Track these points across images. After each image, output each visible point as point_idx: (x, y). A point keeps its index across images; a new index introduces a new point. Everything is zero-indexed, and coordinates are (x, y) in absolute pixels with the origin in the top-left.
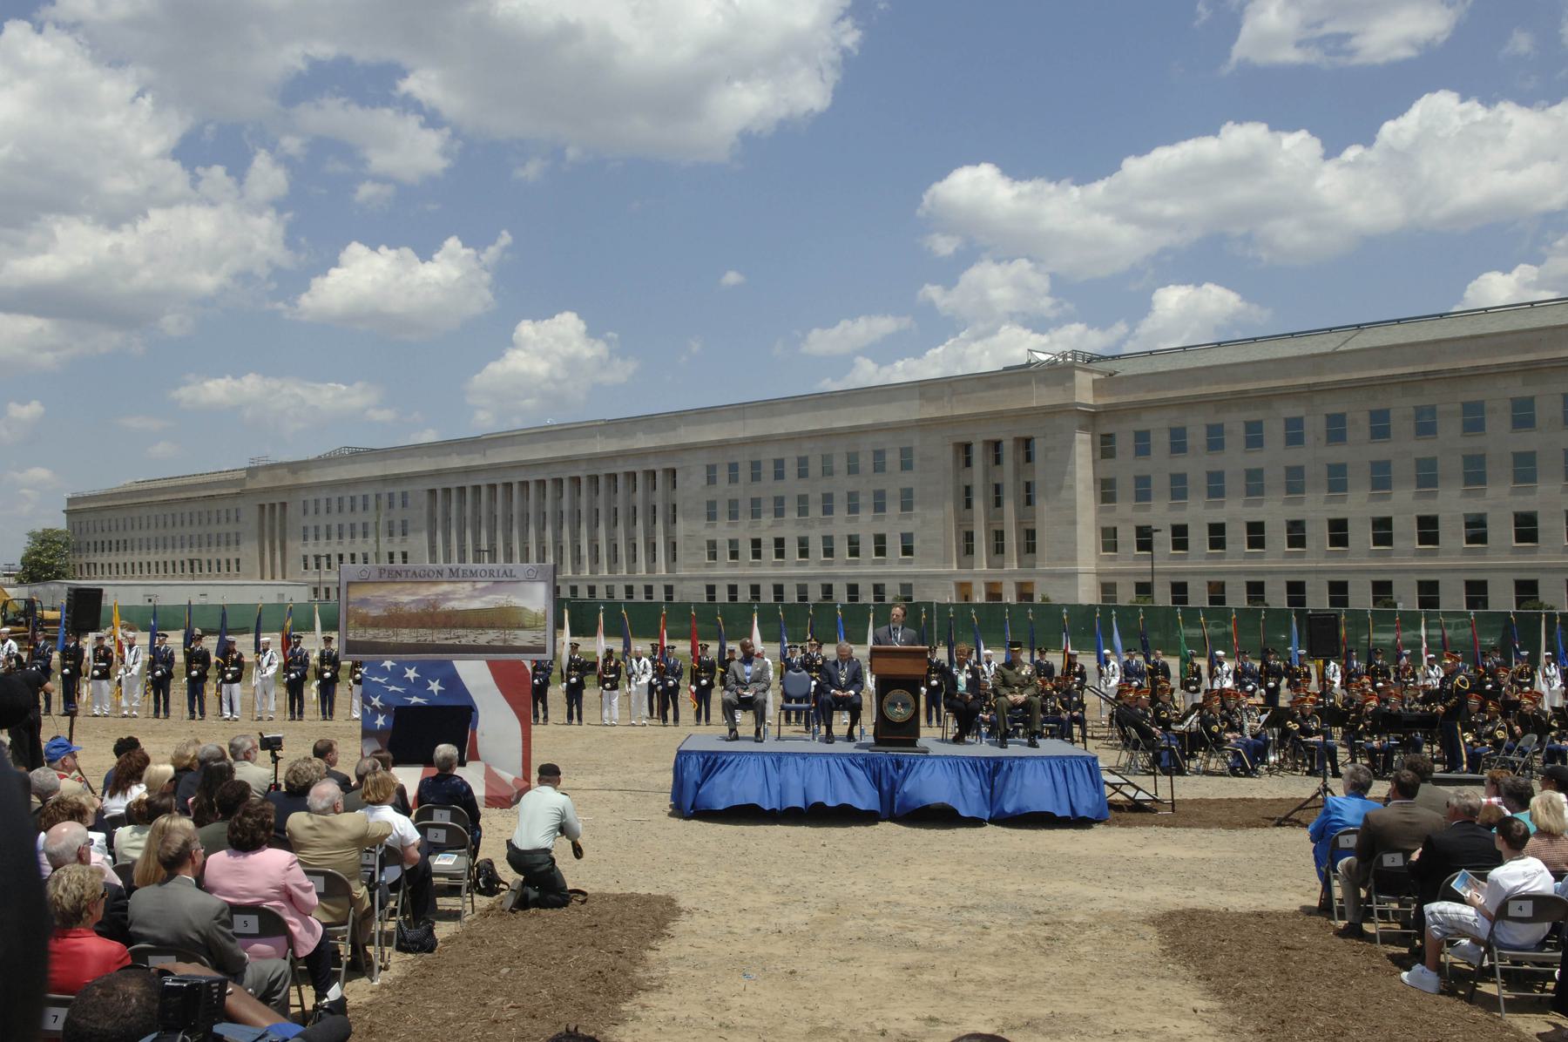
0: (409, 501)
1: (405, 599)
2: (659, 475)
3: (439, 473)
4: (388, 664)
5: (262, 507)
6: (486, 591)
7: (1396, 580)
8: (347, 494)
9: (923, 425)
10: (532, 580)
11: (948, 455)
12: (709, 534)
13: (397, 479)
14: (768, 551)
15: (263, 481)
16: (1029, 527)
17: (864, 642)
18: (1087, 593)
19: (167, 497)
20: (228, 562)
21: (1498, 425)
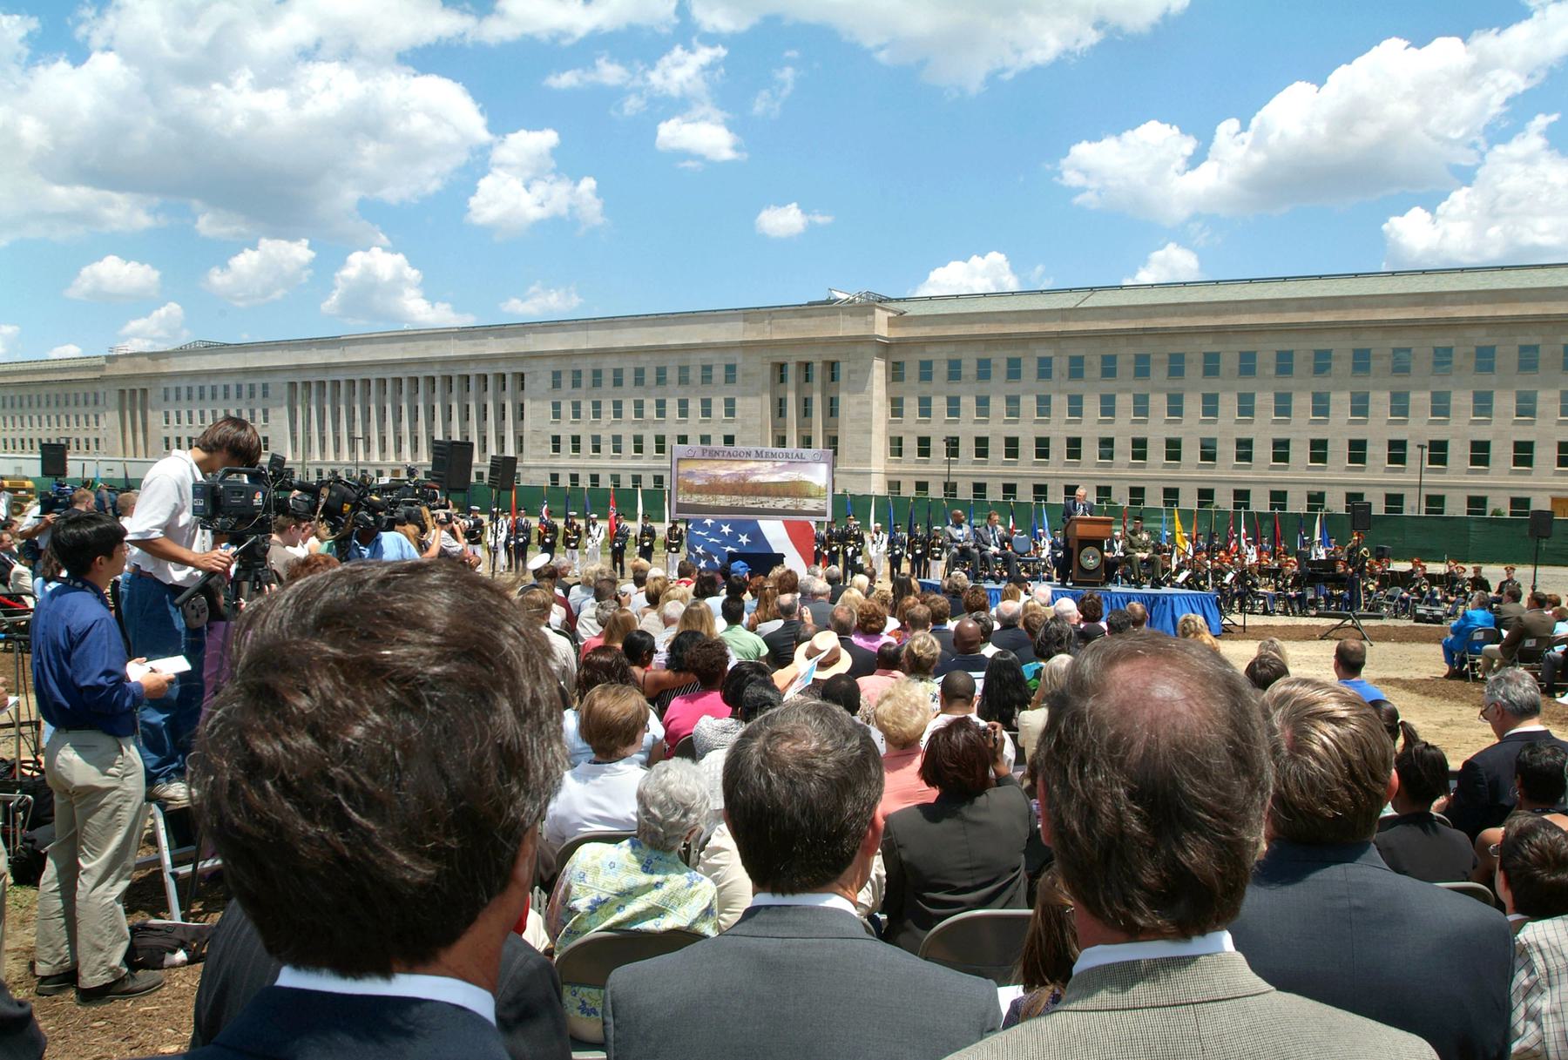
1: (722, 472)
3: (300, 368)
4: (709, 522)
5: (122, 392)
6: (783, 468)
7: (1050, 484)
8: (208, 384)
9: (746, 346)
10: (817, 462)
12: (555, 431)
13: (259, 371)
14: (607, 448)
15: (122, 369)
18: (878, 487)
19: (23, 379)
20: (87, 440)
21: (1194, 370)
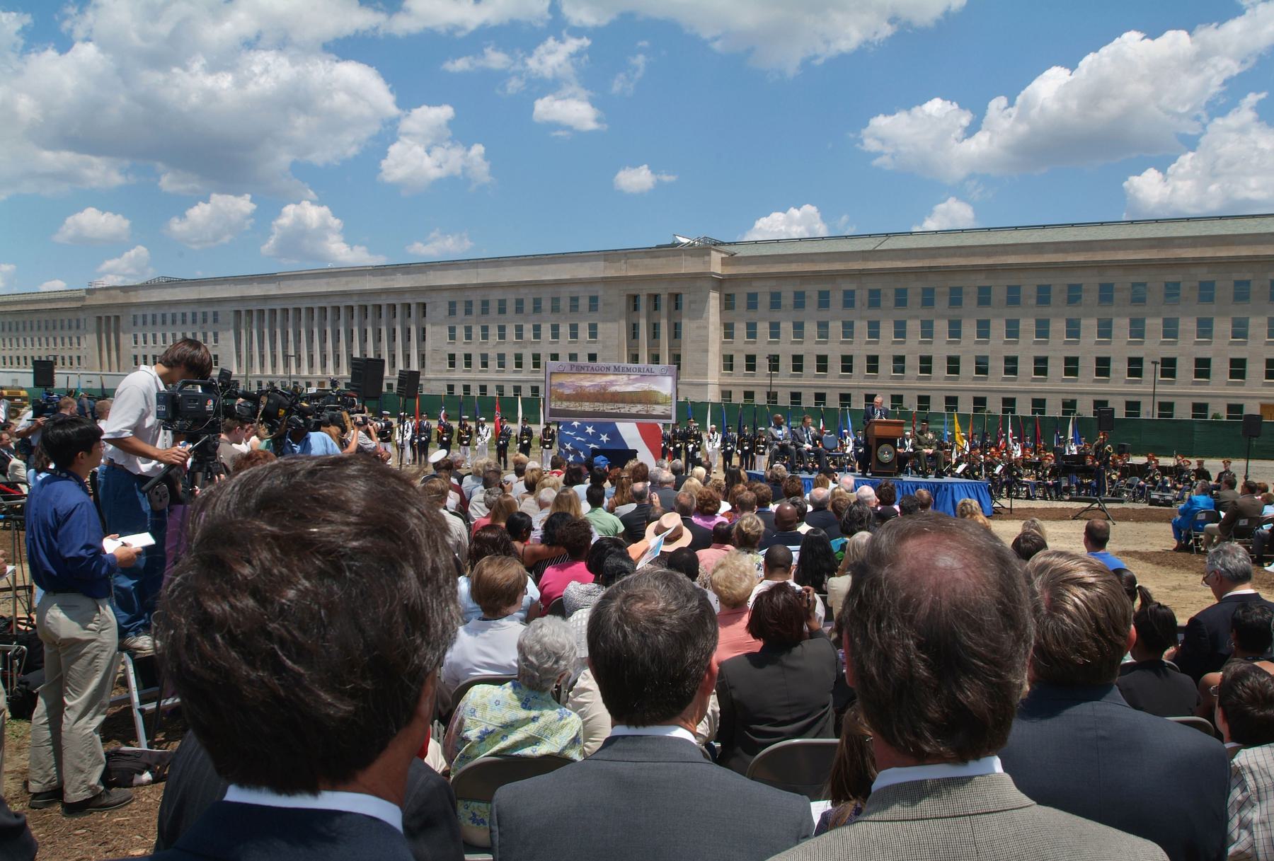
0: (220, 318)
1: (587, 384)
2: (413, 307)
3: (243, 299)
4: (576, 423)
5: (99, 318)
6: (636, 380)
9: (606, 281)
10: (664, 375)
11: (623, 302)
12: (451, 350)
13: (210, 302)
15: (99, 300)
16: (676, 352)
17: (516, 421)
18: (713, 396)
19: (19, 308)
20: (71, 358)
21: (970, 301)
